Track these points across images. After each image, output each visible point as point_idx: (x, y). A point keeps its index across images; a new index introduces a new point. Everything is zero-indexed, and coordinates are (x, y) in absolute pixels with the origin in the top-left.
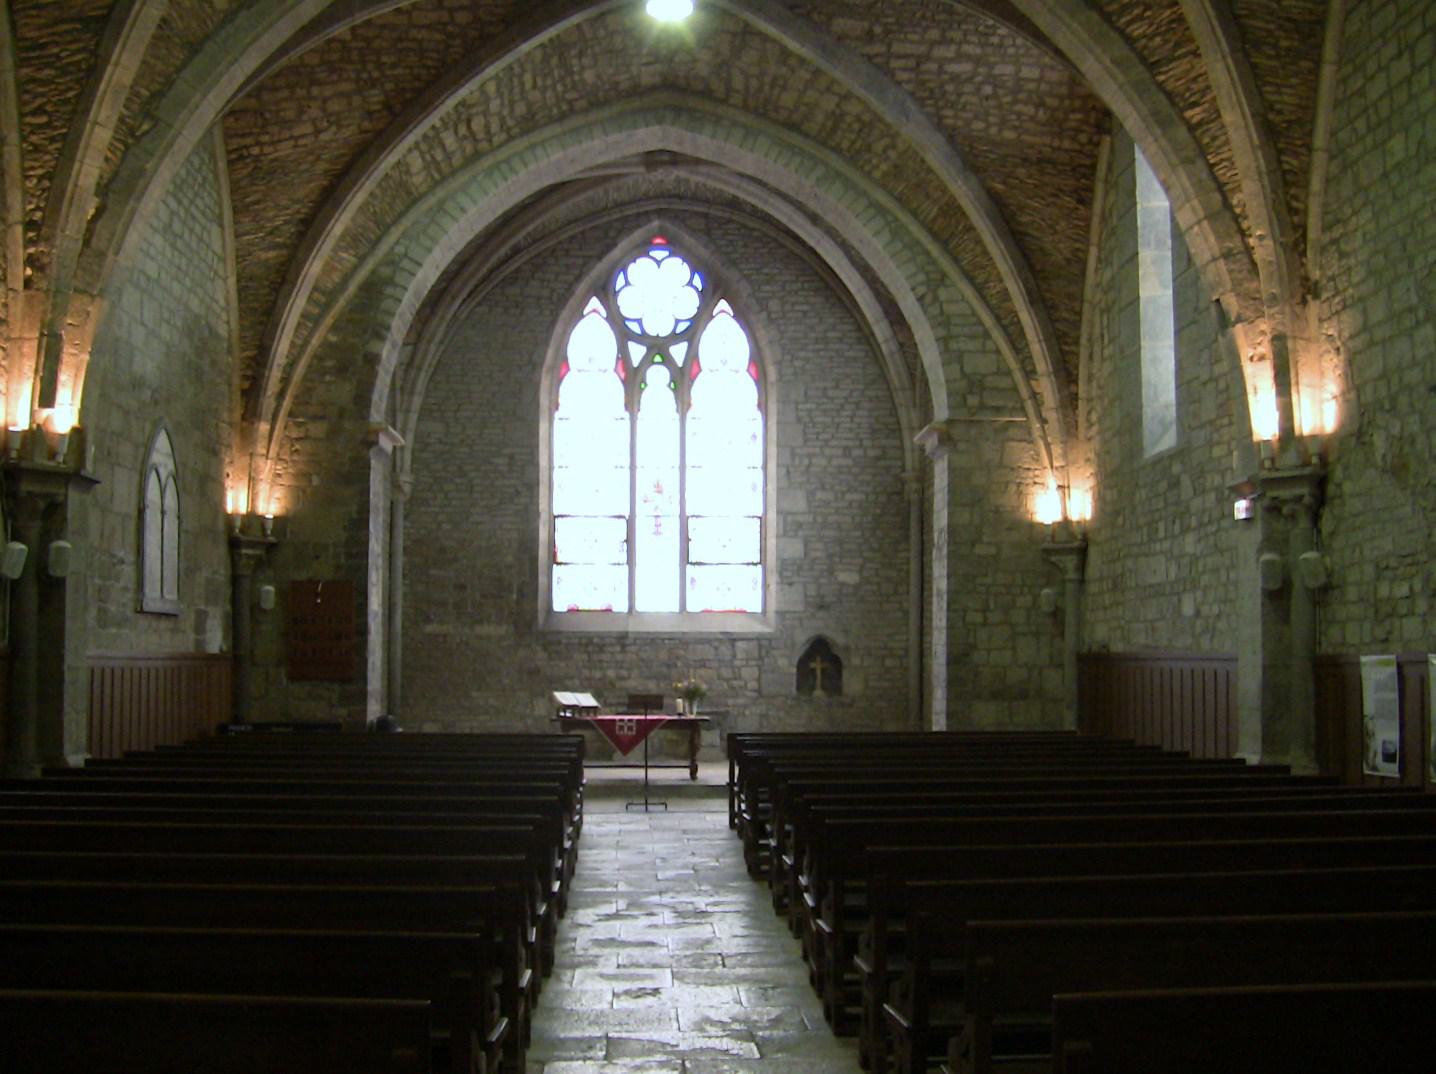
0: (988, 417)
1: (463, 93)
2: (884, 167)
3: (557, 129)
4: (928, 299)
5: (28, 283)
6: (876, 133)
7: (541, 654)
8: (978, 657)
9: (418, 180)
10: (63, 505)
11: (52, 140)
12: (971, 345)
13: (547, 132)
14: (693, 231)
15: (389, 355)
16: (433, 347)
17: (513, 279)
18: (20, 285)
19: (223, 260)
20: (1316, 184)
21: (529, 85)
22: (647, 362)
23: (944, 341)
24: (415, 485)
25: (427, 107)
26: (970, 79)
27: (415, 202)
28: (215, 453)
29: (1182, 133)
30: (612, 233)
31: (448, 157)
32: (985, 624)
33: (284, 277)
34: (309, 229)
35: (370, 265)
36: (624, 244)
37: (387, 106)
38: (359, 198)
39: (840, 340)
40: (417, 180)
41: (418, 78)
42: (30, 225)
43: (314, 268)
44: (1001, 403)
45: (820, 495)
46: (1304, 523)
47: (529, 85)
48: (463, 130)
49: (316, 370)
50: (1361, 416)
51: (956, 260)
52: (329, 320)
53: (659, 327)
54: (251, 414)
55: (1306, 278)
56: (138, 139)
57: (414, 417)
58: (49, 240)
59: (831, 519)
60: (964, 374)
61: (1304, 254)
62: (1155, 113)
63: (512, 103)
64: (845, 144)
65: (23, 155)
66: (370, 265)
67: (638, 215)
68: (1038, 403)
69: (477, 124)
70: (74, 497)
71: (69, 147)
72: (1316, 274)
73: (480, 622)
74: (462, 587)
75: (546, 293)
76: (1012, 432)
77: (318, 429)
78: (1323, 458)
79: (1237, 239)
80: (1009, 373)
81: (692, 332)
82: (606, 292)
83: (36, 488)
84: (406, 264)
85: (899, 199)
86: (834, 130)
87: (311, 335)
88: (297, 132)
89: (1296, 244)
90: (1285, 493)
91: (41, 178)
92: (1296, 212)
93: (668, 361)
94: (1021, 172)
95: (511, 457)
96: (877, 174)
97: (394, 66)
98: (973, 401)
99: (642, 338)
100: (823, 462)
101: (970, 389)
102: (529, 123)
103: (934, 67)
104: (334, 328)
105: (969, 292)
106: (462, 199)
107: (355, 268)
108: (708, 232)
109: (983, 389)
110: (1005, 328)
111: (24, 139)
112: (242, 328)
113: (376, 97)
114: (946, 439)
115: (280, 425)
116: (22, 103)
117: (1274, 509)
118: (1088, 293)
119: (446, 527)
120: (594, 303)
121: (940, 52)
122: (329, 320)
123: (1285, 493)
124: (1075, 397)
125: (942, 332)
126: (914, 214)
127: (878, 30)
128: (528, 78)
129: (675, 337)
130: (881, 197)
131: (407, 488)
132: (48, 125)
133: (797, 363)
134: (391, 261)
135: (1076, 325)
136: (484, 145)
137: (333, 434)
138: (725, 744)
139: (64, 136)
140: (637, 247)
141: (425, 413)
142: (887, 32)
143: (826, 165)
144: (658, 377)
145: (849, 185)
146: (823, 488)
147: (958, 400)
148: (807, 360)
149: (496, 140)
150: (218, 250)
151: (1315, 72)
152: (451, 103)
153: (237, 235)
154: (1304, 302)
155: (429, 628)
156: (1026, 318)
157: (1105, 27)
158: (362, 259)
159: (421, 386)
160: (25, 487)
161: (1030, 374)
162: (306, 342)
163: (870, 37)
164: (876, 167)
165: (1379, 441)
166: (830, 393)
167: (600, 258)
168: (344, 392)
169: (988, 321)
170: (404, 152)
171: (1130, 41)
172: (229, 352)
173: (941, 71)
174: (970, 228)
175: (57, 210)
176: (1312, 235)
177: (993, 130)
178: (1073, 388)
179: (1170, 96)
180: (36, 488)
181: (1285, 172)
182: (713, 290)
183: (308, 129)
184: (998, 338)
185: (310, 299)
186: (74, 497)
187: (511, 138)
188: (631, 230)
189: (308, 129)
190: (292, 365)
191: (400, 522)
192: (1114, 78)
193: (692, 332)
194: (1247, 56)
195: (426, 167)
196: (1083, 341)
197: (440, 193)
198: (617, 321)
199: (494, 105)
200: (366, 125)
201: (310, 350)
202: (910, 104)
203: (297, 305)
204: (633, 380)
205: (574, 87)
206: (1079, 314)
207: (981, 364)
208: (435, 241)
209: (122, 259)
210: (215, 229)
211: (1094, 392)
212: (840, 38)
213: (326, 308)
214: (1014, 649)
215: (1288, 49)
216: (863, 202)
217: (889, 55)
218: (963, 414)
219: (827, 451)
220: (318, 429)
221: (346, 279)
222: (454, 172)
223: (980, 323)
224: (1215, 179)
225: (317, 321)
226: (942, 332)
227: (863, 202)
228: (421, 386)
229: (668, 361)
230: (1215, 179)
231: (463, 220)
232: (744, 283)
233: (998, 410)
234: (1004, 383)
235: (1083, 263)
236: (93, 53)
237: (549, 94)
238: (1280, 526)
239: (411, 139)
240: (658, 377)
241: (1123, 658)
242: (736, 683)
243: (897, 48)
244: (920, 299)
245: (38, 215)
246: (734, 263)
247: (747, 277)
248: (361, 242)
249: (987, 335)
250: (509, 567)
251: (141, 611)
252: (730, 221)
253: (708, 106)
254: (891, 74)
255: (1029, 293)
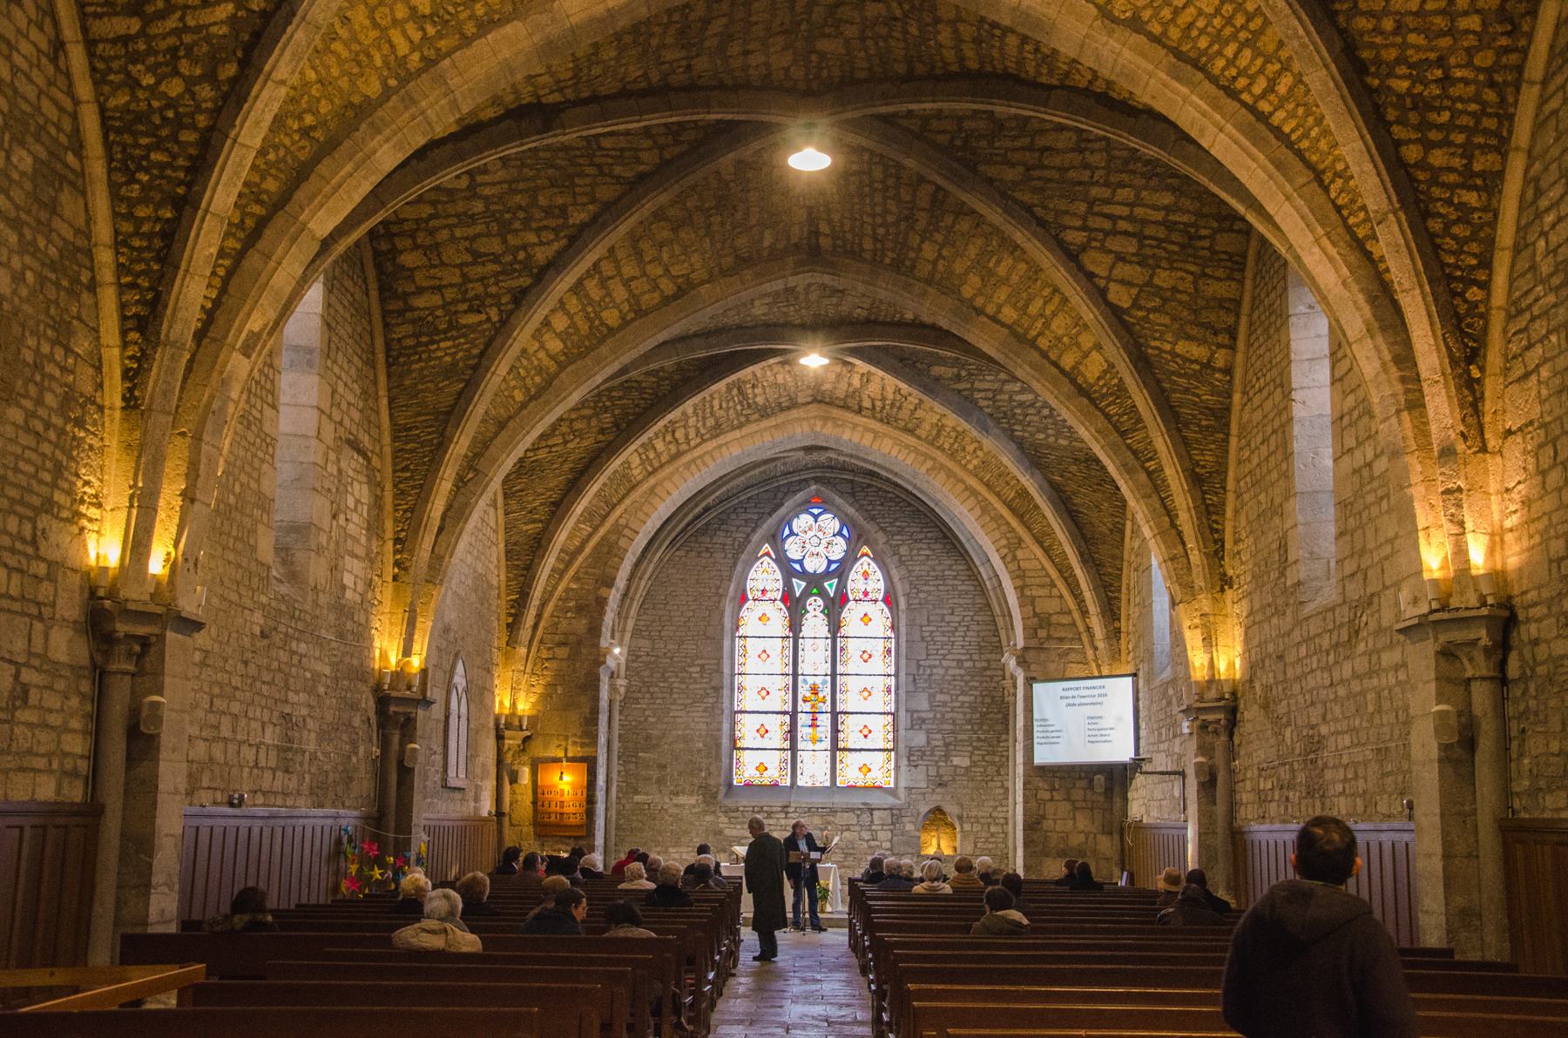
0: (1053, 645)
1: (670, 417)
2: (975, 462)
3: (737, 434)
4: (1008, 559)
5: (395, 578)
6: (967, 439)
7: (723, 819)
8: (1048, 824)
9: (637, 472)
10: (415, 720)
11: (413, 487)
12: (1041, 592)
13: (731, 436)
14: (841, 494)
15: (614, 597)
16: (643, 583)
17: (703, 531)
18: (390, 579)
19: (496, 532)
20: (1229, 513)
21: (716, 407)
22: (807, 593)
23: (1021, 589)
24: (628, 688)
25: (643, 427)
26: (1032, 405)
27: (633, 488)
28: (489, 671)
29: (1143, 477)
30: (780, 495)
31: (658, 455)
32: (1052, 800)
33: (539, 544)
34: (558, 508)
35: (602, 532)
36: (789, 504)
37: (616, 425)
38: (594, 488)
39: (955, 578)
40: (636, 472)
41: (637, 406)
42: (397, 541)
43: (561, 537)
44: (1063, 634)
45: (940, 697)
46: (1223, 738)
47: (716, 407)
48: (669, 438)
49: (562, 610)
50: (1254, 666)
51: (1029, 529)
52: (571, 573)
53: (815, 565)
54: (512, 642)
55: (1225, 574)
56: (465, 484)
57: (628, 635)
58: (411, 552)
59: (948, 716)
60: (1036, 614)
61: (1222, 558)
62: (1124, 465)
63: (704, 419)
64: (946, 446)
65: (395, 497)
66: (602, 532)
67: (800, 481)
68: (1092, 636)
69: (679, 434)
70: (420, 712)
71: (424, 492)
72: (1230, 572)
73: (677, 794)
74: (662, 767)
75: (729, 541)
76: (1072, 657)
77: (562, 652)
78: (1234, 693)
79: (1180, 548)
80: (1070, 612)
81: (840, 570)
82: (776, 539)
83: (400, 709)
84: (626, 532)
85: (987, 485)
86: (938, 435)
87: (558, 583)
88: (550, 443)
89: (1216, 552)
90: (1210, 717)
91: (405, 511)
92: (1217, 531)
93: (823, 593)
94: (1074, 468)
95: (702, 666)
96: (970, 467)
97: (620, 398)
98: (1042, 633)
99: (804, 574)
100: (941, 671)
101: (1039, 624)
102: (718, 430)
103: (1006, 397)
104: (576, 578)
105: (1039, 553)
106: (668, 485)
107: (590, 536)
108: (853, 494)
109: (1050, 624)
110: (1066, 579)
111: (395, 486)
112: (508, 579)
113: (607, 418)
114: (1022, 662)
115: (534, 649)
116: (394, 464)
117: (1204, 727)
118: (1126, 557)
119: (652, 720)
120: (766, 548)
121: (1008, 387)
122: (571, 573)
123: (1210, 717)
124: (1118, 631)
125: (1019, 582)
126: (998, 495)
127: (963, 373)
128: (716, 403)
129: (827, 574)
130: (972, 482)
131: (622, 690)
132: (411, 478)
133: (922, 595)
134: (617, 530)
135: (1119, 577)
136: (684, 447)
137: (571, 658)
138: (846, 888)
139: (421, 486)
140: (800, 505)
141: (637, 633)
142: (970, 375)
143: (934, 459)
144: (815, 605)
145: (950, 474)
146: (942, 692)
147: (1031, 632)
148: (929, 592)
149: (693, 443)
150: (492, 524)
151: (1226, 441)
152: (661, 424)
153: (507, 514)
154: (1222, 590)
155: (638, 798)
156: (1079, 572)
157: (1092, 409)
158: (596, 529)
159: (633, 612)
160: (393, 709)
161: (1084, 613)
162: (555, 588)
163: (958, 378)
164: (969, 462)
165: (1257, 685)
166: (947, 618)
167: (770, 514)
168: (581, 625)
169: (1054, 574)
170: (630, 455)
171: (1108, 416)
172: (499, 597)
173: (1011, 399)
174: (1036, 507)
175: (416, 531)
176: (1227, 546)
177: (1052, 439)
178: (1117, 624)
179: (1134, 453)
180: (400, 709)
181: (1207, 506)
182: (856, 538)
183: (559, 440)
184: (1062, 586)
185: (558, 558)
186: (420, 712)
187: (704, 441)
188: (795, 493)
189: (559, 440)
190: (543, 605)
191: (617, 717)
192: (1312, 231)
193: (840, 570)
194: (1179, 430)
195: (642, 463)
196: (1124, 590)
197: (652, 481)
198: (783, 562)
199: (692, 421)
200: (601, 437)
201: (557, 594)
202: (990, 423)
203: (550, 561)
204: (794, 607)
205: (749, 406)
206: (1121, 569)
207: (1051, 606)
208: (648, 515)
209: (454, 560)
210: (492, 510)
211: (1131, 628)
212: (937, 379)
213: (569, 564)
214: (1074, 819)
215: (1208, 427)
216: (961, 487)
217: (972, 390)
218: (1033, 643)
219: (945, 663)
220: (562, 652)
221: (584, 542)
222: (662, 466)
223: (1048, 575)
224: (1165, 507)
225: (562, 573)
226: (1019, 582)
227: (961, 487)
228: (633, 612)
229: (823, 593)
230: (1165, 507)
231: (668, 500)
232: (880, 534)
233: (1061, 640)
234: (1065, 620)
235: (1122, 532)
236: (442, 435)
237: (731, 412)
238: (1209, 739)
239: (633, 447)
240: (815, 605)
241: (1150, 827)
242: (873, 843)
243: (977, 385)
244: (1003, 558)
245: (403, 534)
246: (873, 518)
247: (883, 529)
248: (595, 517)
249: (1053, 585)
250: (699, 751)
251: (445, 786)
252: (869, 486)
253: (849, 416)
254: (975, 402)
255: (1082, 555)
